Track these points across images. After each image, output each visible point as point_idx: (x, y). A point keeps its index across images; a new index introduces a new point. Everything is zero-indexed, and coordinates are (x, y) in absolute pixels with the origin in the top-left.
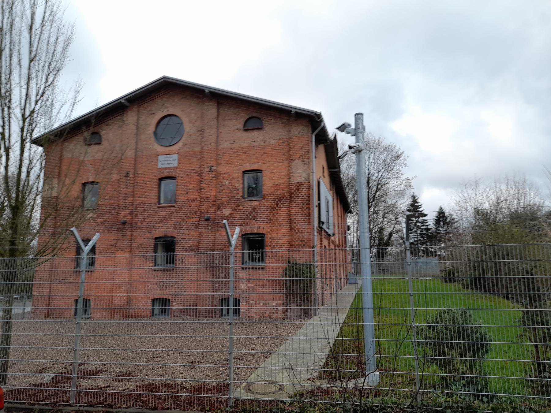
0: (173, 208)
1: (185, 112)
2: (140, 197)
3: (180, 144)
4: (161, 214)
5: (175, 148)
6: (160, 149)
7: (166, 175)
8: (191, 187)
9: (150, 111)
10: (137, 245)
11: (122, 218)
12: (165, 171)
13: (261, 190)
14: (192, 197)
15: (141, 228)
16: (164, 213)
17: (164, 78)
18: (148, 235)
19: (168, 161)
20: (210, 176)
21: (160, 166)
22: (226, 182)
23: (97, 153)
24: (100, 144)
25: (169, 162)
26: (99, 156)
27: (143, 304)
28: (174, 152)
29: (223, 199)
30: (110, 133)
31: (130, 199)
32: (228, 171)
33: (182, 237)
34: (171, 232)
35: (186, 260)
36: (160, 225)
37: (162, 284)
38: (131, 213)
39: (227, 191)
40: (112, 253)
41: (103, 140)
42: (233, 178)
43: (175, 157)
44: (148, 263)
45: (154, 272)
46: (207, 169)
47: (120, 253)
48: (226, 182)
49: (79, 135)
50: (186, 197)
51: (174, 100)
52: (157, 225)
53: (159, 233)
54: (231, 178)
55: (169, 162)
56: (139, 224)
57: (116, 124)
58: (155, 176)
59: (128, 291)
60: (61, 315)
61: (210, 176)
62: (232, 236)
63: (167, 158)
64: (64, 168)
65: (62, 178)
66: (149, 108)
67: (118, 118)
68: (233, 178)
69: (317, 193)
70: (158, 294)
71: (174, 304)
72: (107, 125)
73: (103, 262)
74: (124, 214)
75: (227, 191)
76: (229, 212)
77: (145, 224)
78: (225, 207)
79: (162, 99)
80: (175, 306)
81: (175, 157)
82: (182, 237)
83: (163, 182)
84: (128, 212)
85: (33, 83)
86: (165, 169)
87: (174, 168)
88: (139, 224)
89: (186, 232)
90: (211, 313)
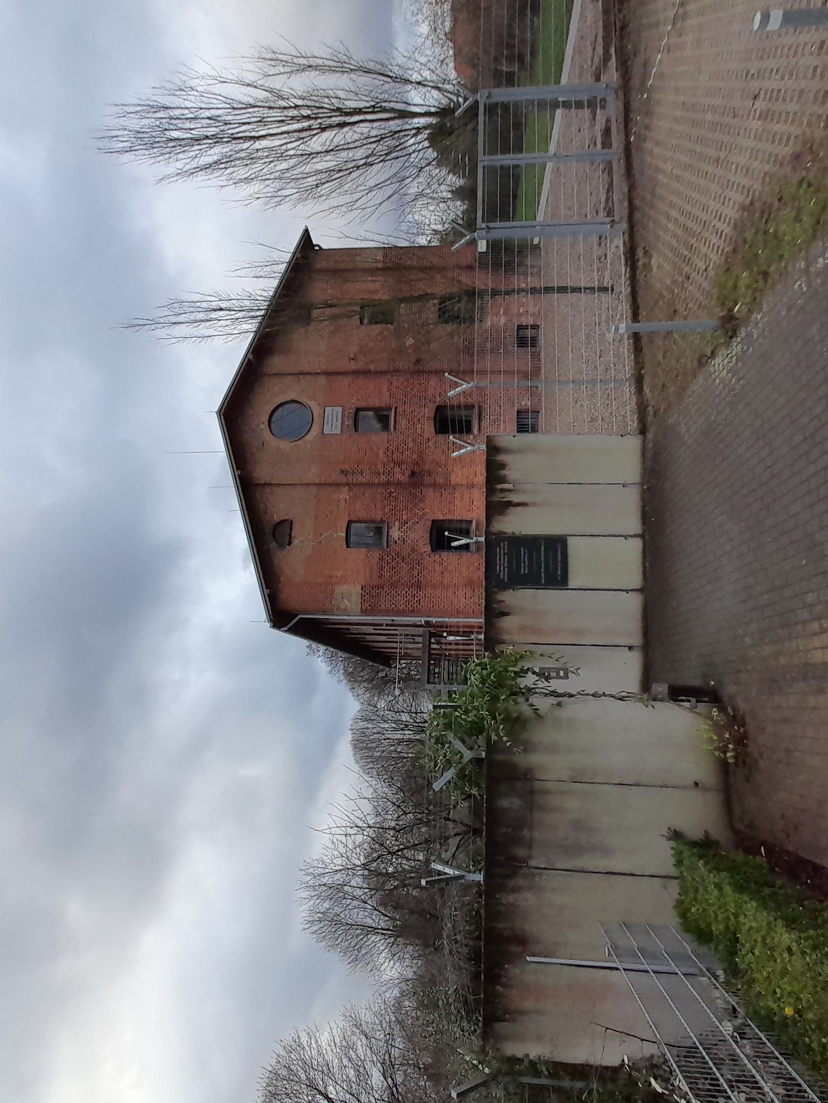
1: (270, 395)
3: (312, 404)
4: (404, 426)
5: (317, 411)
6: (315, 431)
12: (346, 423)
13: (380, 303)
14: (385, 388)
15: (421, 454)
17: (219, 412)
18: (431, 444)
19: (333, 420)
21: (338, 431)
22: (371, 344)
24: (292, 522)
25: (335, 419)
28: (322, 412)
31: (380, 466)
33: (438, 397)
34: (429, 412)
36: (419, 426)
40: (448, 39)
41: (287, 518)
51: (251, 416)
52: (419, 431)
53: (429, 428)
55: (335, 419)
57: (267, 499)
58: (351, 436)
62: (445, 874)
66: (254, 450)
67: (258, 496)
74: (400, 475)
80: (526, 403)
82: (438, 397)
83: (361, 413)
84: (397, 469)
85: (219, 106)
87: (343, 411)
88: (415, 456)
89: (431, 392)
90: (536, 356)
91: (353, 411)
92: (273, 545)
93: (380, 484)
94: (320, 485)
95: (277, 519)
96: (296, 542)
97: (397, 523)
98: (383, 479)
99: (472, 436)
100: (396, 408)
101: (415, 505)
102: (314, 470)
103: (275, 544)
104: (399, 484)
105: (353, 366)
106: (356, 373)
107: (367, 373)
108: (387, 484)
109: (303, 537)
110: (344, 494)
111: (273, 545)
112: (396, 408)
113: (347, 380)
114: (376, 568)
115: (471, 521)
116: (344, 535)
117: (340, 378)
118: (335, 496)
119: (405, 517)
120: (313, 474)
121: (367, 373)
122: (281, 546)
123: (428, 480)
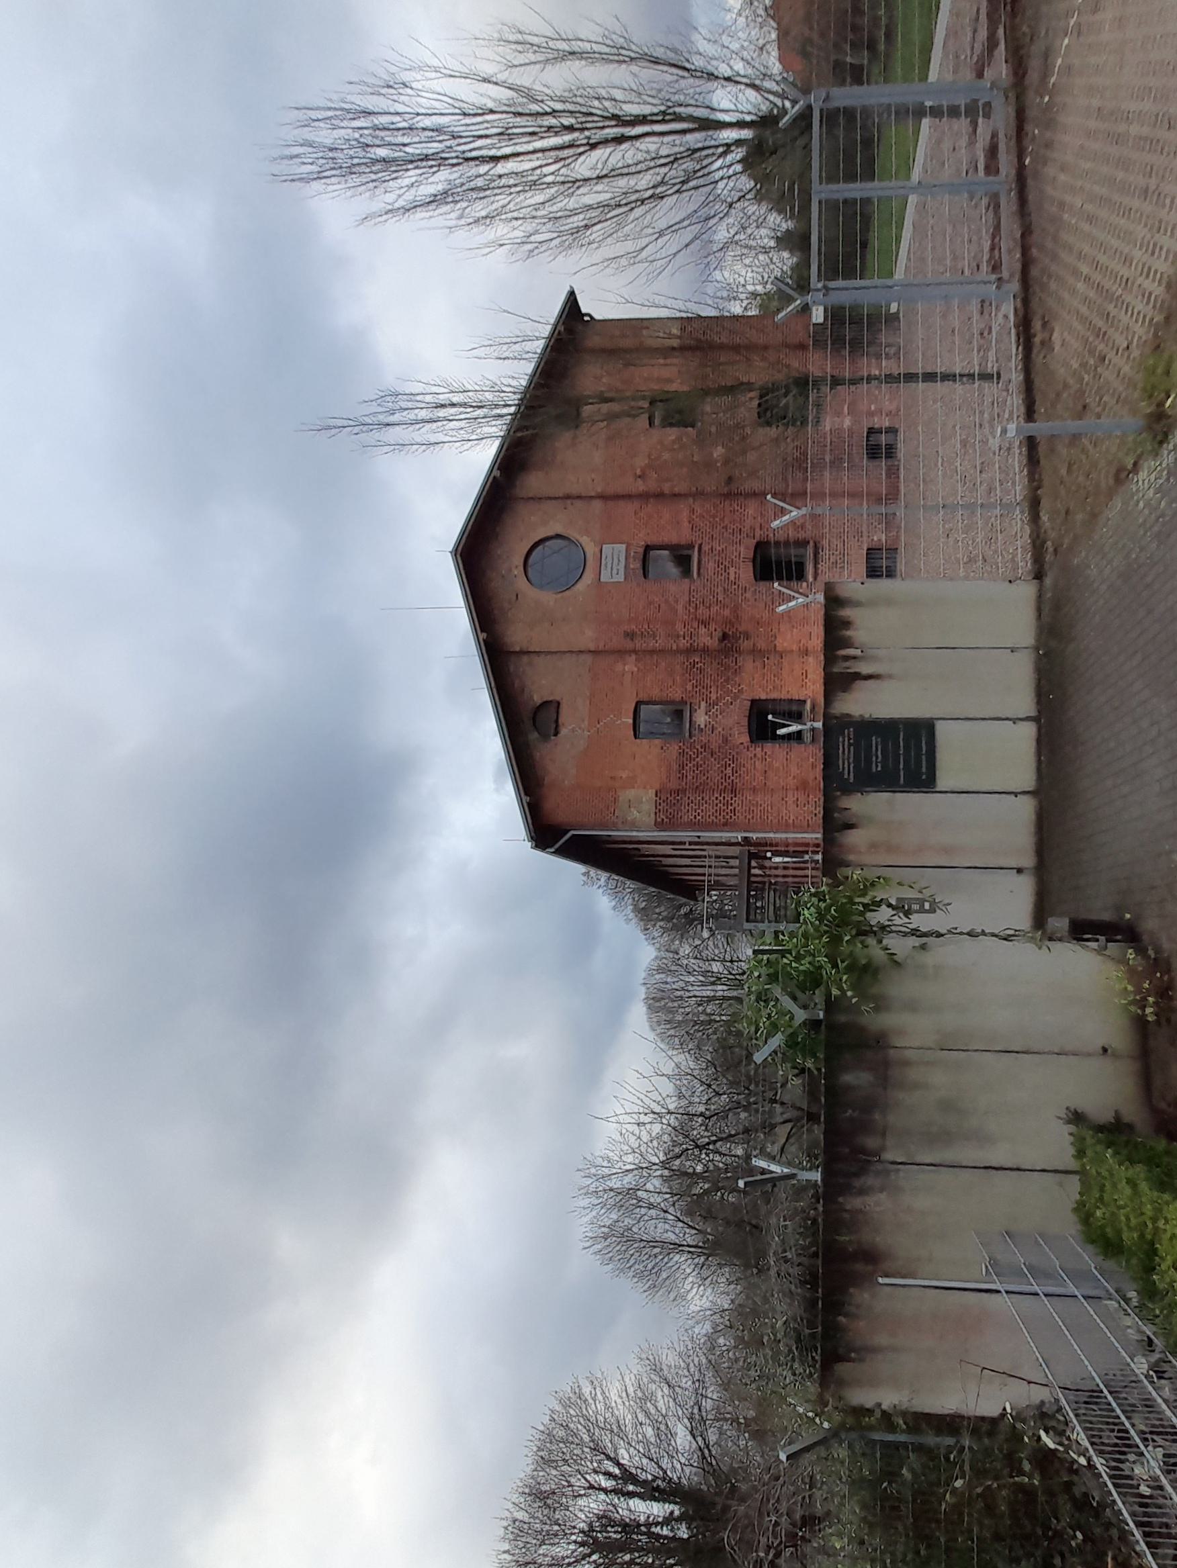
5: (591, 549)
15: (736, 609)
16: (711, 565)
18: (748, 595)
24: (559, 703)
28: (597, 550)
30: (540, 684)
31: (679, 627)
34: (745, 550)
36: (732, 570)
38: (705, 623)
43: (607, 548)
52: (732, 577)
56: (727, 612)
67: (512, 669)
72: (523, 690)
74: (707, 638)
80: (880, 537)
81: (607, 548)
84: (703, 630)
88: (727, 612)
89: (749, 522)
90: (893, 472)
91: (641, 550)
92: (534, 736)
93: (679, 651)
94: (595, 652)
95: (537, 699)
96: (564, 731)
97: (703, 704)
98: (683, 643)
99: (805, 584)
100: (700, 546)
101: (727, 681)
102: (589, 633)
103: (536, 734)
104: (705, 651)
105: (640, 486)
106: (645, 497)
107: (659, 496)
108: (690, 651)
109: (575, 726)
110: (630, 665)
111: (534, 736)
112: (700, 546)
113: (628, 508)
114: (675, 767)
115: (805, 701)
116: (631, 721)
117: (621, 503)
118: (619, 667)
119: (714, 696)
120: (588, 637)
121: (659, 496)
122: (545, 737)
123: (745, 645)
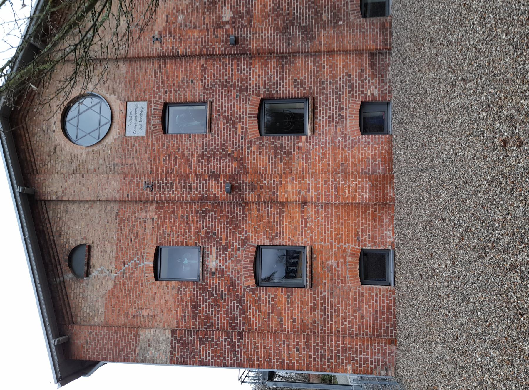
0: (214, 104)
2: (190, 166)
7: (158, 121)
8: (182, 76)
9: (49, 156)
10: (269, 166)
11: (220, 194)
15: (242, 161)
16: (221, 120)
18: (254, 148)
20: (168, 39)
21: (142, 133)
22: (181, 18)
23: (105, 252)
24: (90, 247)
26: (110, 249)
27: (371, 146)
28: (122, 107)
29: (206, 22)
30: (76, 228)
31: (192, 179)
32: (164, 16)
34: (251, 107)
35: (299, 78)
36: (240, 125)
37: (336, 118)
38: (215, 176)
39: (194, 16)
41: (84, 242)
42: (176, 7)
43: (131, 106)
44: (300, 144)
45: (317, 132)
46: (157, 45)
47: (282, 195)
48: (181, 18)
49: (69, 291)
50: (199, 83)
52: (239, 132)
53: (251, 128)
54: (174, 11)
56: (235, 165)
57: (61, 218)
58: (158, 139)
59: (347, 176)
60: (390, 311)
61: (168, 39)
63: (130, 121)
64: (123, 320)
65: (141, 321)
66: (46, 157)
68: (176, 7)
69: (261, 128)
70: (353, 124)
71: (369, 93)
72: (60, 235)
73: (296, 229)
74: (216, 190)
75: (194, 16)
76: (228, 11)
77: (236, 155)
78: (220, 17)
79: (34, 135)
80: (372, 91)
81: (131, 106)
84: (213, 183)
86: (148, 123)
87: (149, 107)
88: (235, 165)
89: (254, 79)
